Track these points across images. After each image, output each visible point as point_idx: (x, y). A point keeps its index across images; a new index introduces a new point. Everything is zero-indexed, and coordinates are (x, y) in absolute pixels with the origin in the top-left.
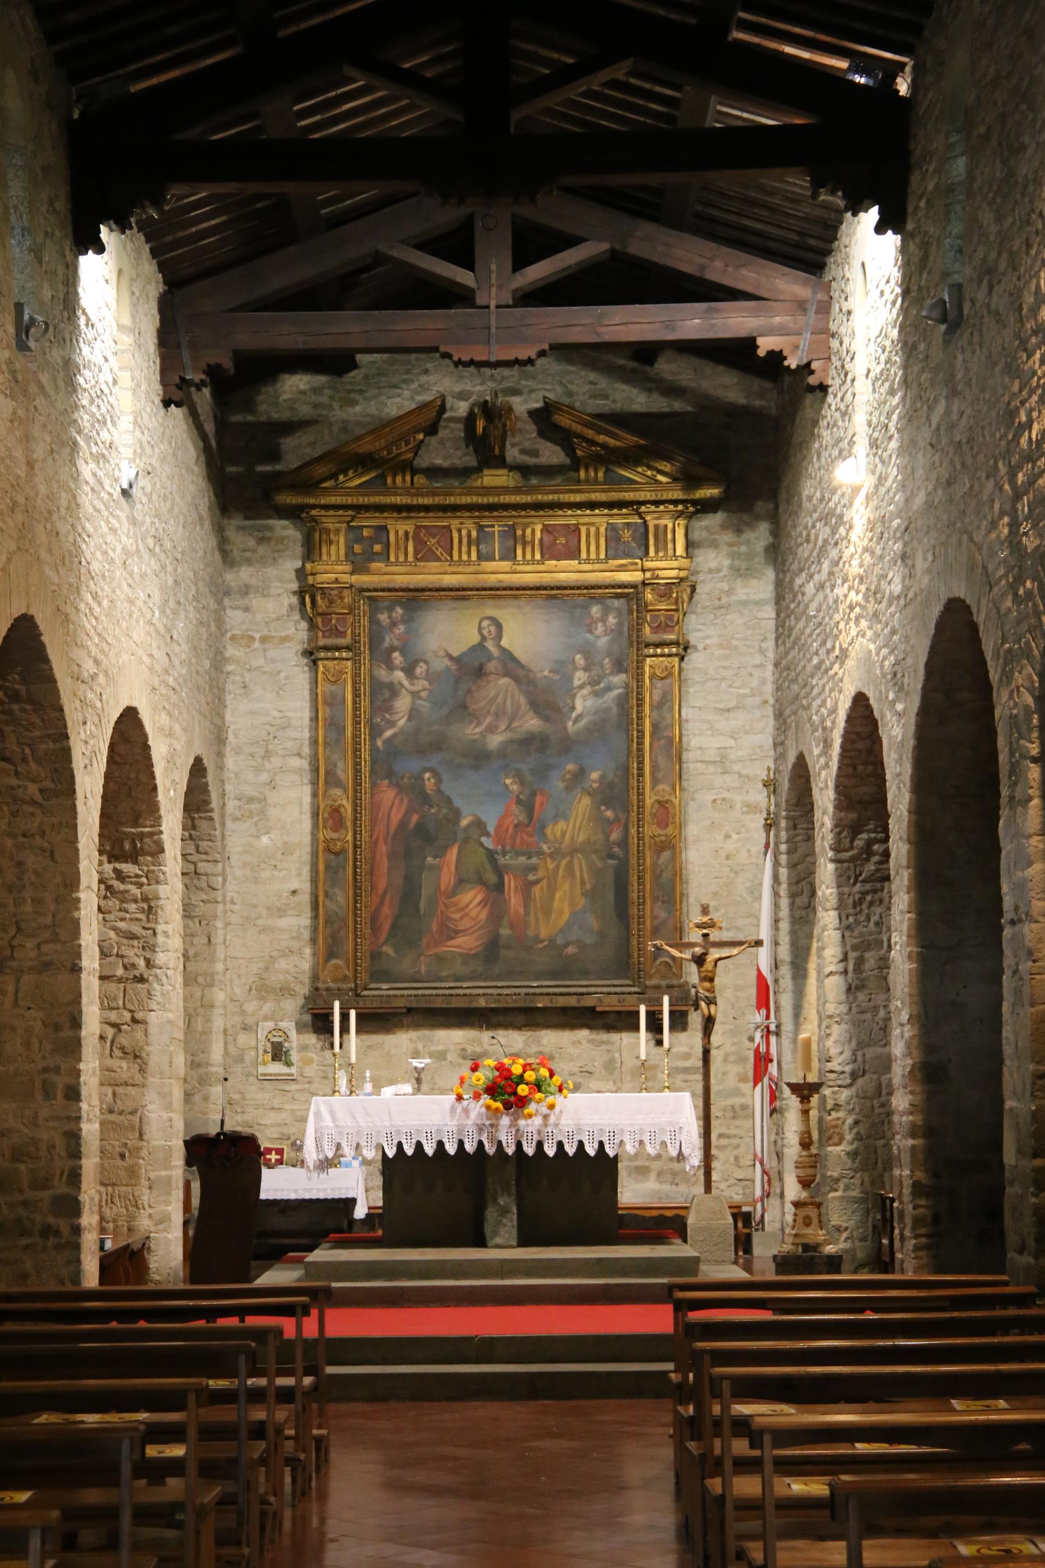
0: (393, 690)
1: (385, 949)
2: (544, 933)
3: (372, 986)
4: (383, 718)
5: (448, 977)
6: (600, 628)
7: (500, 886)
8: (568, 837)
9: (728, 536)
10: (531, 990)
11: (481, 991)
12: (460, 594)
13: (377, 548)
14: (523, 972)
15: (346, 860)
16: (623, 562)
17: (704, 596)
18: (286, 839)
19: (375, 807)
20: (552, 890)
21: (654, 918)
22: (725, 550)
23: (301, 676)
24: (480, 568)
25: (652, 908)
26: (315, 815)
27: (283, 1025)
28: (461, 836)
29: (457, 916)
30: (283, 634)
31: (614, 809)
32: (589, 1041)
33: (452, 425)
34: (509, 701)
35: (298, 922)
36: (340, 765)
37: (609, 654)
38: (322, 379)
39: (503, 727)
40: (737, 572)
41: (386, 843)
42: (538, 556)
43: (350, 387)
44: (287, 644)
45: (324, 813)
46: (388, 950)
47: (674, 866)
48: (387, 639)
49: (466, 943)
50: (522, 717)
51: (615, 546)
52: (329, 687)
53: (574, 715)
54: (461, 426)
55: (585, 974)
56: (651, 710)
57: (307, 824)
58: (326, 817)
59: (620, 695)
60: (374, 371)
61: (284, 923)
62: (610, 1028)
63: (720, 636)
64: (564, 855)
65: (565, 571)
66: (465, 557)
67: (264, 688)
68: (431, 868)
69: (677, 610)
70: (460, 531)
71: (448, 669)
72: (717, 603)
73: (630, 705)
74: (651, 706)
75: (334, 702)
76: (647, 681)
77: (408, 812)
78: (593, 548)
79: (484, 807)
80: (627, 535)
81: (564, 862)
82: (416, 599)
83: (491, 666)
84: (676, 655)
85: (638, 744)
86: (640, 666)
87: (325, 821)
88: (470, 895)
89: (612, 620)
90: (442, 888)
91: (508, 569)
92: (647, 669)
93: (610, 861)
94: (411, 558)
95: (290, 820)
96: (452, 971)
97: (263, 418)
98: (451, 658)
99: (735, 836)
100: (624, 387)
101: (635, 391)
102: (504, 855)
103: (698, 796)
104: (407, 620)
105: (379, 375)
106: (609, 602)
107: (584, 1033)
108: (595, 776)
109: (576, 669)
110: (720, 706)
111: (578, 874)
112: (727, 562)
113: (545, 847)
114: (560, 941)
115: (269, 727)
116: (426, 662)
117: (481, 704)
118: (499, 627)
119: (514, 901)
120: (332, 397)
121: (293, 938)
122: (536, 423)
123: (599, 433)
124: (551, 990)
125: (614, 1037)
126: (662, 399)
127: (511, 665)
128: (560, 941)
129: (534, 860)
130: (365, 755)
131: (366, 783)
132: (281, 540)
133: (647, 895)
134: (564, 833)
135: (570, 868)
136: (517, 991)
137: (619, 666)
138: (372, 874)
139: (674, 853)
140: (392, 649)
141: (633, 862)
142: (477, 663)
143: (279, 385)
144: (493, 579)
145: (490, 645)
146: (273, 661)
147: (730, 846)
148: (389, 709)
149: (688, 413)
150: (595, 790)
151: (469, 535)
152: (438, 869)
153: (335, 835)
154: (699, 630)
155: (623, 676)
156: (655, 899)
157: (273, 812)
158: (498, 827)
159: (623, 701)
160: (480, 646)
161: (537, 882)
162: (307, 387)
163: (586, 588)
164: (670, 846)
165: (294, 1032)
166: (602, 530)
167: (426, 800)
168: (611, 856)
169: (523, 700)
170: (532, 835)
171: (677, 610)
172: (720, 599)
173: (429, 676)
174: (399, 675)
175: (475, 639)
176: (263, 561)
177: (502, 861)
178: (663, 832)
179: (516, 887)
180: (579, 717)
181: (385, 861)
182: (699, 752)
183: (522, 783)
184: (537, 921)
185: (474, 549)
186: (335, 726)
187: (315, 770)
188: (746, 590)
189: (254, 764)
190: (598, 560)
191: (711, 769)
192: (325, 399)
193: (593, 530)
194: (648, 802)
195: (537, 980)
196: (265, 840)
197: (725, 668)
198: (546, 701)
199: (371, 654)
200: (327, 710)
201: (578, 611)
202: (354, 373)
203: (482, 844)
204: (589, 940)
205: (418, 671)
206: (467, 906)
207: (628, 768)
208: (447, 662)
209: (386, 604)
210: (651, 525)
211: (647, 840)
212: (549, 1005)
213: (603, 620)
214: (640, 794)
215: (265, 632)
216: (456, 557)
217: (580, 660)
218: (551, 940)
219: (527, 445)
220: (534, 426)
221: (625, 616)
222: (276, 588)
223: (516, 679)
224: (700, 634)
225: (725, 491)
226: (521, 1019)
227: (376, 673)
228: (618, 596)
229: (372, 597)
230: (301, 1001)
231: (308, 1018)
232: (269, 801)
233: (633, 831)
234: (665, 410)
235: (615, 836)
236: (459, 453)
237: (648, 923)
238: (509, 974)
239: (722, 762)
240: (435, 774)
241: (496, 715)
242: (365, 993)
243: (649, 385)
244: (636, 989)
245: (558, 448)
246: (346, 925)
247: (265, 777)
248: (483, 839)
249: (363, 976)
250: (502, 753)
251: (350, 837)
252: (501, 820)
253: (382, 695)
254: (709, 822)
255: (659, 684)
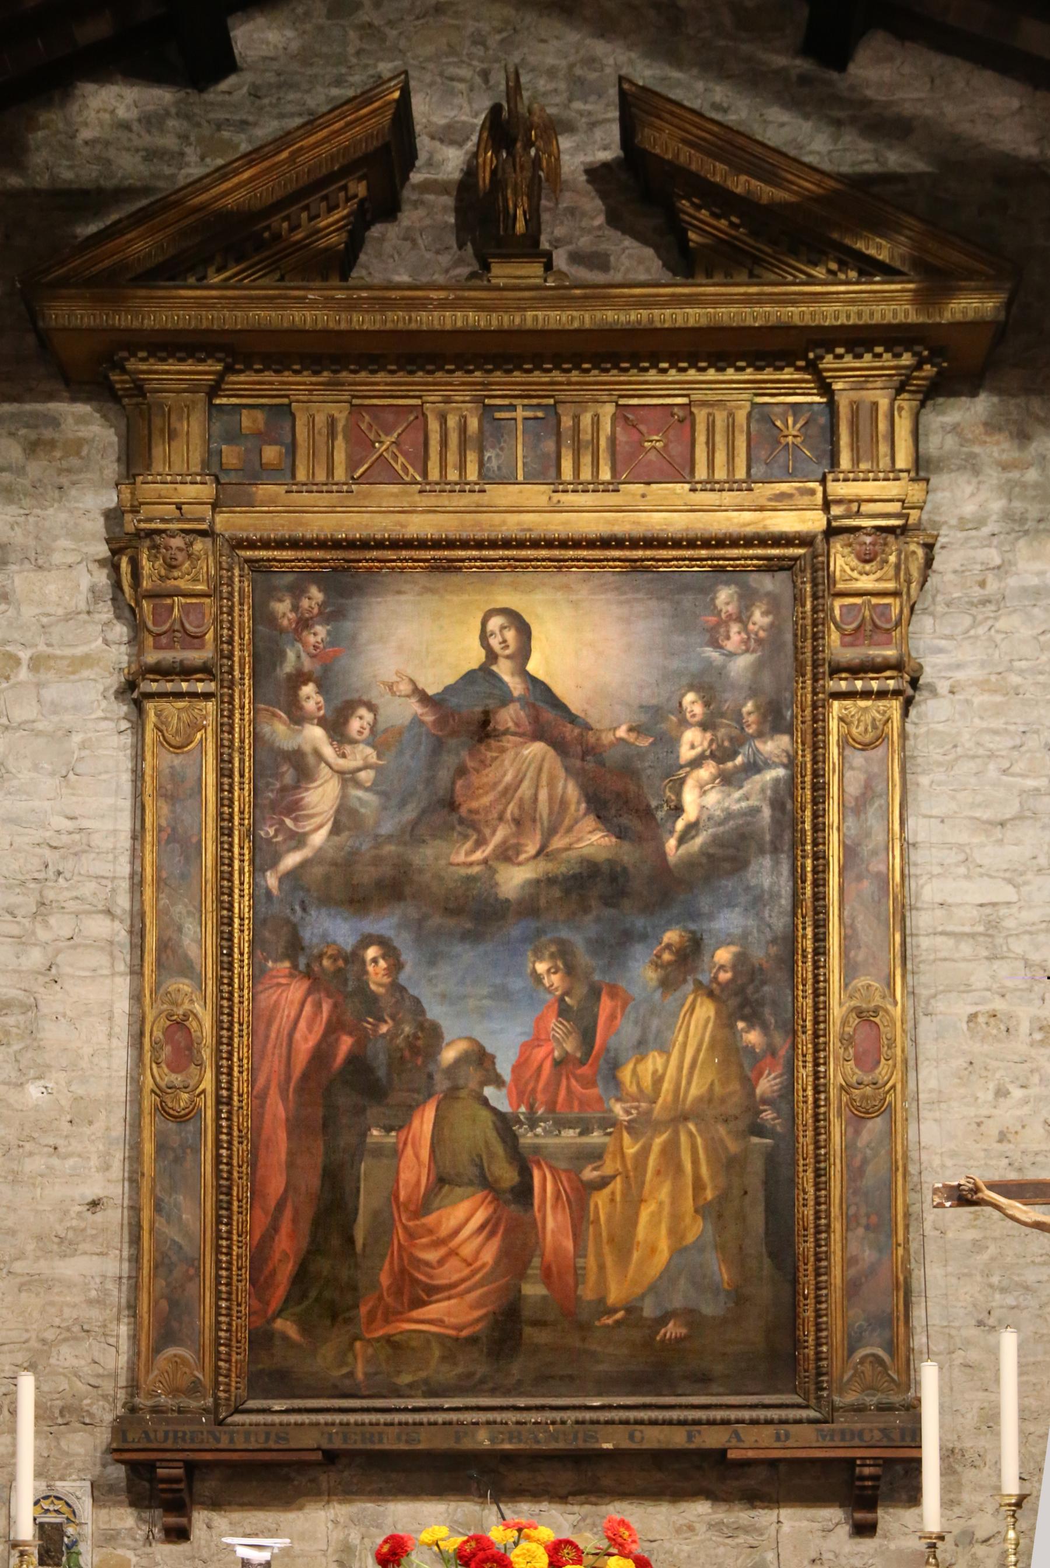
0: (303, 766)
1: (279, 1324)
2: (615, 1295)
3: (251, 1404)
4: (281, 827)
5: (410, 1386)
6: (735, 636)
7: (523, 1193)
8: (666, 1086)
9: (998, 448)
10: (588, 1415)
11: (482, 1417)
12: (445, 558)
13: (271, 453)
14: (571, 1378)
15: (200, 1133)
16: (784, 487)
17: (950, 577)
18: (81, 1091)
19: (262, 1018)
20: (634, 1201)
21: (849, 1262)
22: (993, 476)
23: (115, 741)
24: (484, 499)
25: (844, 1240)
26: (137, 1038)
27: (63, 1487)
28: (442, 1084)
29: (432, 1256)
30: (79, 651)
31: (765, 1028)
32: (711, 1526)
33: (430, 197)
34: (543, 795)
35: (99, 1267)
36: (190, 927)
37: (754, 692)
38: (163, 96)
39: (531, 849)
40: (1017, 525)
41: (285, 1099)
42: (605, 475)
43: (221, 115)
44: (86, 673)
45: (155, 1030)
46: (286, 1326)
47: (892, 1151)
48: (291, 655)
49: (451, 1313)
50: (570, 830)
51: (768, 453)
52: (169, 760)
53: (680, 825)
54: (449, 201)
55: (703, 1380)
56: (842, 818)
57: (121, 1056)
58: (162, 1041)
59: (777, 781)
60: (270, 77)
61: (71, 1268)
62: (754, 1498)
63: (983, 664)
64: (657, 1127)
65: (666, 510)
66: (453, 475)
67: (36, 767)
68: (379, 1151)
69: (896, 594)
70: (443, 419)
71: (417, 721)
72: (977, 592)
73: (797, 820)
74: (842, 804)
75: (177, 791)
76: (834, 750)
77: (334, 1028)
78: (720, 457)
79: (493, 1023)
80: (792, 428)
81: (658, 1141)
82: (350, 570)
83: (508, 717)
84: (897, 693)
85: (815, 884)
86: (818, 719)
87: (156, 1047)
88: (461, 1210)
89: (759, 618)
90: (403, 1195)
91: (542, 501)
92: (833, 725)
93: (755, 1140)
94: (340, 474)
95: (87, 1050)
96: (423, 1374)
97: (42, 182)
98: (424, 698)
99: (1017, 1093)
100: (785, 117)
101: (807, 126)
102: (533, 1126)
103: (939, 1005)
104: (333, 614)
105: (279, 86)
106: (754, 579)
107: (700, 1509)
108: (724, 955)
109: (684, 723)
110: (986, 815)
111: (688, 1167)
112: (997, 505)
113: (618, 1109)
114: (649, 1311)
115: (47, 852)
116: (371, 707)
117: (486, 800)
118: (524, 631)
119: (553, 1223)
120: (184, 138)
121: (90, 1302)
122: (603, 195)
123: (739, 170)
124: (632, 1415)
125: (765, 1517)
126: (866, 145)
127: (549, 715)
128: (649, 1311)
129: (596, 1137)
130: (242, 906)
131: (242, 970)
132: (76, 447)
133: (835, 1211)
134: (658, 1081)
135: (671, 1151)
136: (558, 1416)
137: (775, 719)
138: (254, 1165)
139: (892, 1121)
140: (301, 677)
141: (806, 1141)
142: (479, 709)
143: (75, 108)
144: (511, 525)
145: (504, 670)
146: (56, 708)
147: (1007, 1114)
148: (294, 808)
149: (920, 176)
150: (724, 986)
151: (463, 428)
152: (396, 1153)
153: (177, 1079)
154: (941, 651)
155: (784, 740)
156: (850, 1222)
157: (52, 1033)
158: (517, 1069)
159: (782, 800)
160: (485, 673)
161: (603, 1183)
162: (134, 114)
163: (706, 543)
164: (877, 1106)
165: (88, 1501)
166: (741, 416)
167: (370, 1003)
168: (758, 1129)
169: (572, 791)
170: (593, 1084)
171: (896, 594)
172: (982, 584)
173: (376, 738)
174: (315, 734)
175: (475, 657)
176: (36, 491)
177: (527, 1138)
178: (867, 1079)
179: (557, 1196)
180: (693, 827)
181: (282, 1135)
182: (939, 913)
183: (570, 971)
184: (602, 1267)
185: (472, 457)
186: (179, 841)
187: (138, 934)
188: (1038, 566)
189: (15, 930)
190: (732, 485)
191: (966, 948)
192: (169, 142)
193: (720, 418)
194: (836, 1011)
195: (599, 1394)
196: (34, 1091)
197: (995, 732)
198: (621, 788)
199: (255, 686)
200: (165, 809)
201: (687, 600)
202: (232, 80)
203: (485, 1102)
204: (709, 1309)
205: (355, 725)
206: (456, 1232)
207: (794, 940)
208: (415, 707)
209: (290, 578)
210: (843, 402)
211: (833, 1092)
212: (626, 1444)
213: (742, 618)
214: (819, 993)
215: (42, 648)
216: (434, 475)
217: (692, 704)
218: (631, 1309)
219: (584, 242)
220: (598, 203)
221: (786, 611)
222: (64, 550)
223: (560, 746)
224: (941, 659)
225: (1008, 305)
226: (566, 1477)
227: (266, 729)
228: (772, 566)
229: (263, 564)
230: (103, 1436)
231: (118, 1473)
232: (44, 1009)
233: (805, 1074)
234: (870, 168)
235: (767, 1085)
236: (445, 259)
237: (837, 1272)
238: (543, 1381)
239: (989, 931)
240: (389, 951)
241: (518, 822)
242: (237, 1418)
243: (841, 114)
244: (812, 1414)
245: (649, 252)
246: (199, 1273)
247: (35, 957)
248: (489, 1091)
249: (237, 1385)
250: (529, 906)
251: (208, 1083)
252: (526, 1048)
253: (282, 778)
254: (961, 1062)
255: (858, 759)
